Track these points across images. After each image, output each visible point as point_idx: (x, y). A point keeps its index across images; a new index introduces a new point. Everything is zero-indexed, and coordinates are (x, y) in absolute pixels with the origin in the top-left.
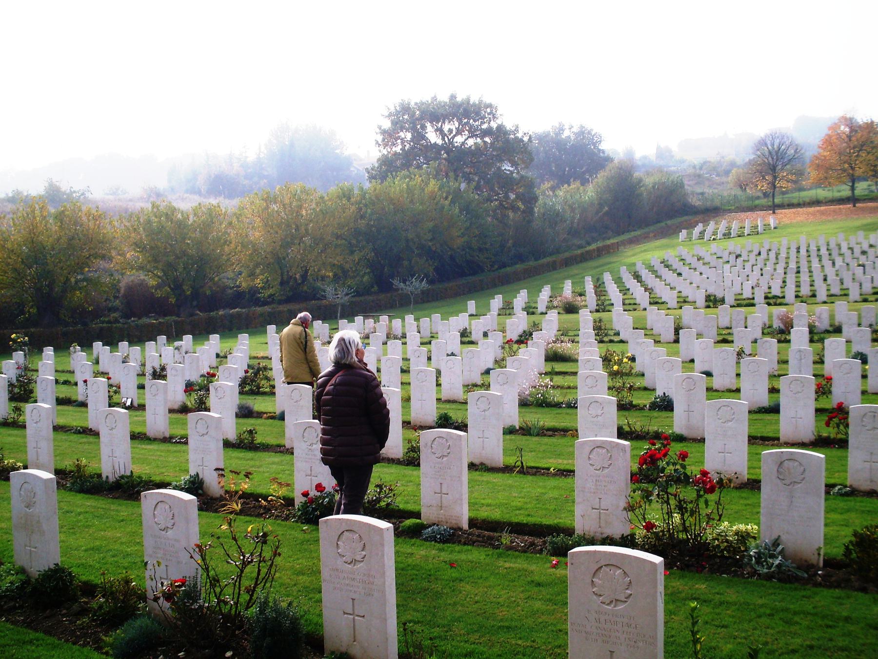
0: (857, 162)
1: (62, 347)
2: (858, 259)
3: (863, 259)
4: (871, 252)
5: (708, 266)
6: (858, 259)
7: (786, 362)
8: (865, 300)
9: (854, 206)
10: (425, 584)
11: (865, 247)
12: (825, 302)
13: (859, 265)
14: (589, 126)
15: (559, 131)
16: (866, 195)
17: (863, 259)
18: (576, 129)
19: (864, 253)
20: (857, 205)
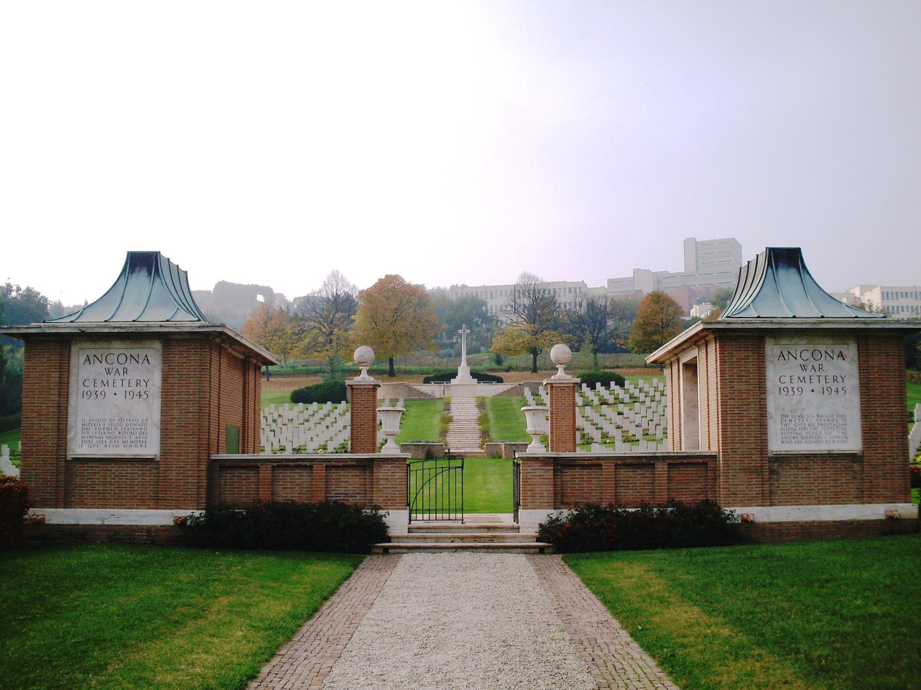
0: (271, 345)
1: (206, 494)
2: (270, 425)
3: (274, 426)
4: (279, 420)
5: (595, 427)
6: (270, 425)
7: (664, 433)
8: (337, 452)
9: (268, 380)
10: (166, 656)
11: (276, 417)
12: (332, 453)
13: (271, 431)
14: (31, 286)
15: (7, 292)
16: (277, 371)
17: (274, 426)
18: (23, 288)
19: (274, 421)
20: (270, 379)
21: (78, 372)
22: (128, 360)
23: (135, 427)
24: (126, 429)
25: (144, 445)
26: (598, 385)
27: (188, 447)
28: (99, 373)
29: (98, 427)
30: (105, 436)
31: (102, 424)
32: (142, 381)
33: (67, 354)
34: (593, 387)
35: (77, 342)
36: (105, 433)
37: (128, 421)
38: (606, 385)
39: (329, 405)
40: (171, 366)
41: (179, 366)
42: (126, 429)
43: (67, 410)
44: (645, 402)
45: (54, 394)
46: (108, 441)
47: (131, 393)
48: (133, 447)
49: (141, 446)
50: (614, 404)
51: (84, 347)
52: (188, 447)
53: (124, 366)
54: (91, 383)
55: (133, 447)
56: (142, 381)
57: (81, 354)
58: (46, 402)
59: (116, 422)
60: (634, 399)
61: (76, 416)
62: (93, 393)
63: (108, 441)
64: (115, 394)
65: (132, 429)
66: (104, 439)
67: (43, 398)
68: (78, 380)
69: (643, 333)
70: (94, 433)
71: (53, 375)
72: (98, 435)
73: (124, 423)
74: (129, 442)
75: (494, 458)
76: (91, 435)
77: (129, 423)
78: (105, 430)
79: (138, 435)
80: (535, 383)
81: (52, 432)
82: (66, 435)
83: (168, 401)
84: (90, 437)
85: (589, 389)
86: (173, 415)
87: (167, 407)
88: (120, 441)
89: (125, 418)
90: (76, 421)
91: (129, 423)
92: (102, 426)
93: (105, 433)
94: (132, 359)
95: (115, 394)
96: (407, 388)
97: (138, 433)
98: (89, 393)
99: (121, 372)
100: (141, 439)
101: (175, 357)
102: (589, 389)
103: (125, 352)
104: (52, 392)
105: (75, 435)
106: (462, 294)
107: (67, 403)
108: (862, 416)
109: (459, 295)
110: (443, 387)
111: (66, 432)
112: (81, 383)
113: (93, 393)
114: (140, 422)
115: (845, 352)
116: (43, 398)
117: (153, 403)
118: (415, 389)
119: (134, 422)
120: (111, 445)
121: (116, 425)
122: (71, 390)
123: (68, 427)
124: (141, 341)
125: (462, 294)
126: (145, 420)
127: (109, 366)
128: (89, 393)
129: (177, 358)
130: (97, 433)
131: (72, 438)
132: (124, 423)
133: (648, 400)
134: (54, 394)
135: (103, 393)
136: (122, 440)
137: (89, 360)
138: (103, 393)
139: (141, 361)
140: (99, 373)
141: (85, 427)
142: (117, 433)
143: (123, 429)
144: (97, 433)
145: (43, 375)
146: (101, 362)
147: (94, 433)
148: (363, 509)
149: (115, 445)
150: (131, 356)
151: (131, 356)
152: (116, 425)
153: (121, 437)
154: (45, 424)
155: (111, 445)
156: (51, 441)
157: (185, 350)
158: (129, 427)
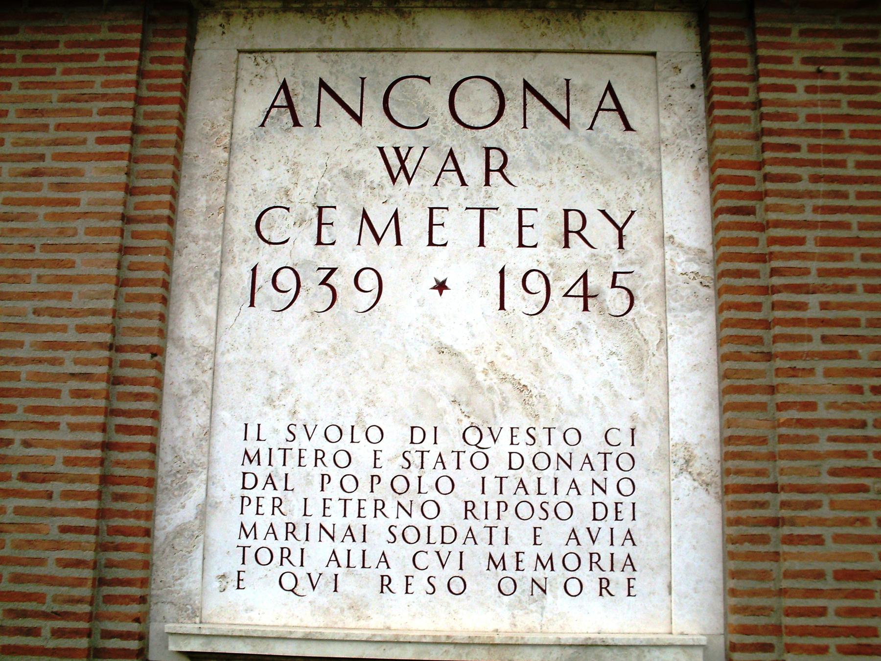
21: (228, 163)
22: (513, 109)
23: (565, 477)
24: (510, 485)
25: (618, 578)
27: (18, 562)
28: (347, 174)
29: (336, 474)
30: (378, 526)
31: (363, 452)
32: (596, 221)
33: (175, 108)
35: (228, 15)
36: (379, 508)
37: (522, 437)
40: (770, 132)
41: (815, 133)
42: (510, 485)
43: (160, 368)
45: (89, 279)
46: (400, 553)
47: (535, 282)
48: (556, 599)
49: (604, 587)
51: (261, 43)
52: (18, 562)
53: (488, 138)
54: (300, 222)
55: (556, 599)
56: (596, 221)
57: (245, 76)
58: (45, 320)
59: (449, 442)
61: (212, 407)
62: (311, 280)
63: (400, 553)
64: (441, 286)
65: (547, 486)
66: (378, 542)
67: (23, 296)
68: (224, 209)
70: (315, 508)
71: (92, 172)
72: (336, 520)
73: (499, 451)
74: (528, 561)
76: (296, 517)
77: (528, 453)
78: (383, 491)
79: (582, 520)
81: (67, 495)
82: (149, 516)
83: (766, 324)
84: (291, 530)
86: (810, 406)
87: (769, 357)
88: (476, 556)
89: (504, 422)
90: (208, 433)
91: (528, 453)
92: (363, 468)
93: (379, 508)
94: (535, 107)
95: (441, 286)
97: (583, 504)
98: (286, 280)
99: (473, 168)
100: (602, 547)
101: (792, 89)
103: (491, 66)
104: (82, 264)
105: (204, 512)
107: (162, 333)
108: (734, 574)
111: (151, 499)
112: (242, 225)
113: (311, 280)
114: (593, 444)
115: (155, 602)
116: (23, 296)
117: (664, 340)
119: (558, 447)
120: (419, 583)
121: (450, 460)
122: (183, 264)
123: (162, 469)
124: (579, 14)
126: (621, 437)
127: (403, 138)
128: (286, 280)
129: (801, 96)
130: (336, 508)
131: (180, 532)
132: (499, 451)
134: (89, 279)
135: (368, 281)
136: (483, 548)
137: (291, 106)
138: (368, 281)
139: (581, 115)
140: (347, 174)
141: (262, 472)
142: (452, 508)
143: (492, 485)
144: (336, 508)
145: (36, 173)
146: (359, 119)
147: (315, 508)
149: (441, 577)
150: (527, 86)
151: (527, 86)
152: (450, 460)
153: (482, 535)
154: (27, 444)
155: (419, 583)
156: (57, 546)
157: (839, 53)
158: (529, 477)
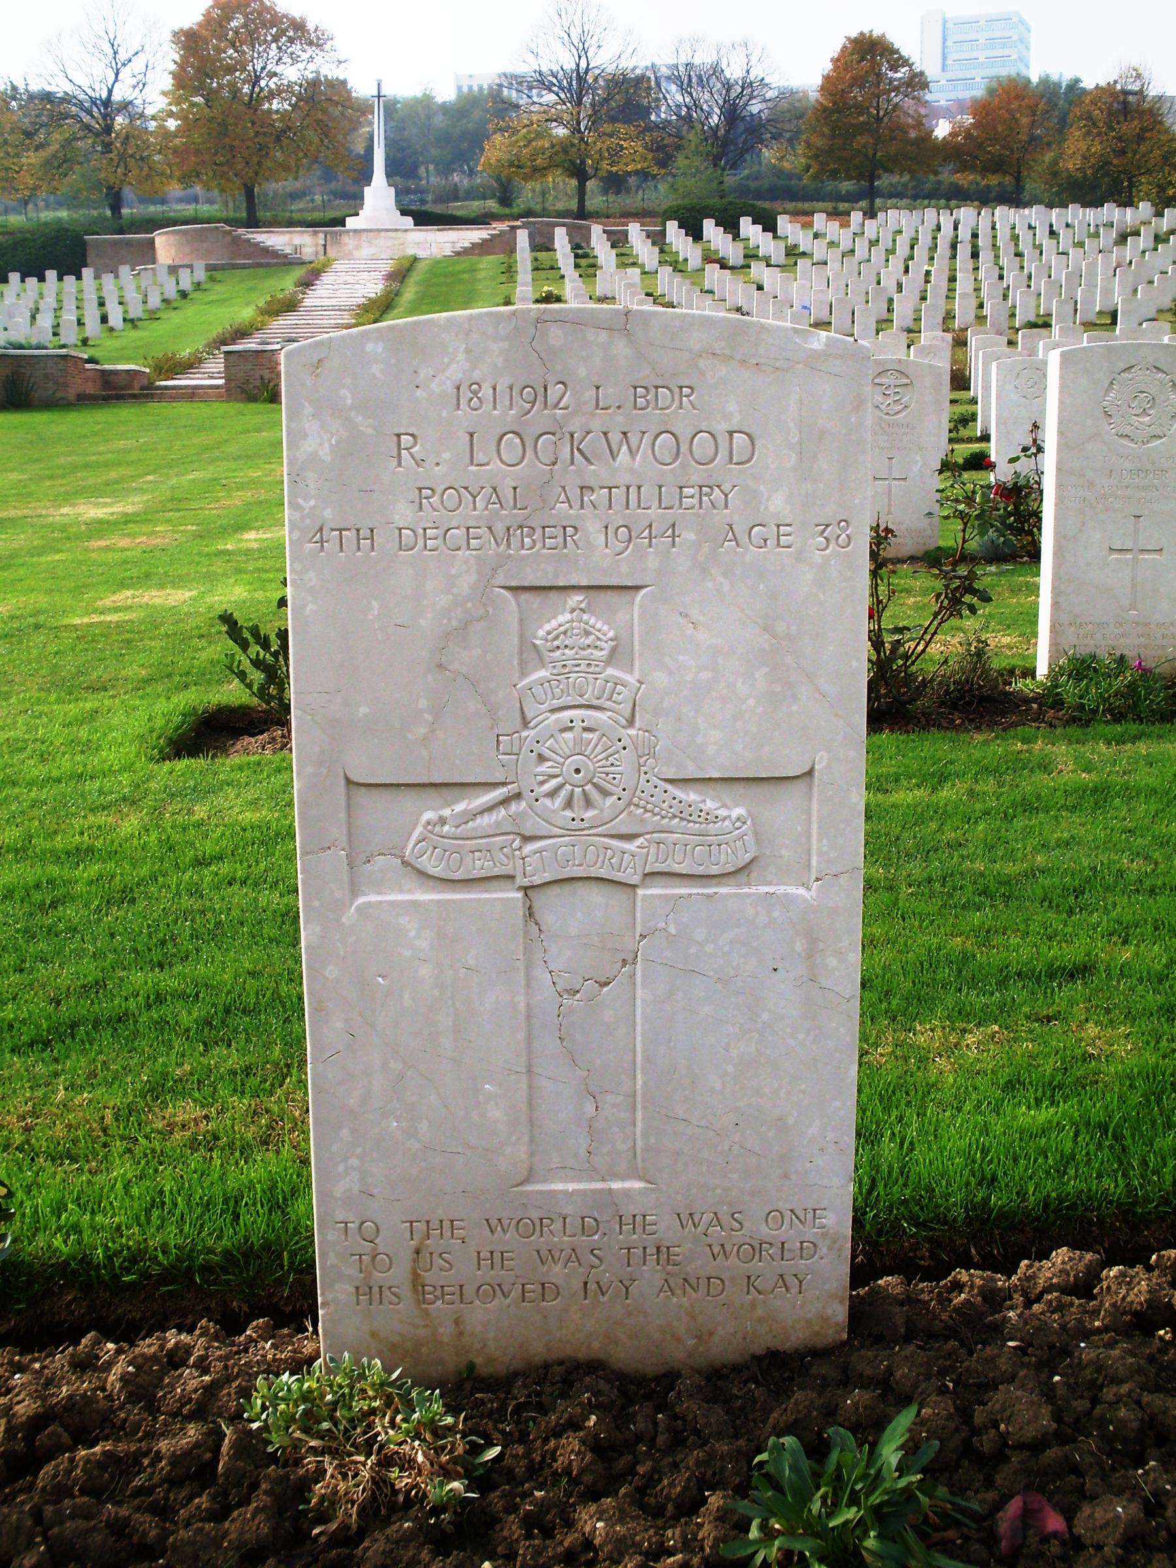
26: (709, 226)
34: (696, 234)
38: (731, 226)
39: (409, 220)
44: (825, 263)
50: (743, 267)
60: (793, 252)
69: (833, 130)
75: (252, 399)
80: (548, 224)
85: (760, 227)
96: (229, 238)
102: (760, 227)
106: (470, 87)
109: (465, 89)
110: (322, 236)
118: (248, 240)
125: (470, 87)
133: (833, 256)
148: (921, 1480)
